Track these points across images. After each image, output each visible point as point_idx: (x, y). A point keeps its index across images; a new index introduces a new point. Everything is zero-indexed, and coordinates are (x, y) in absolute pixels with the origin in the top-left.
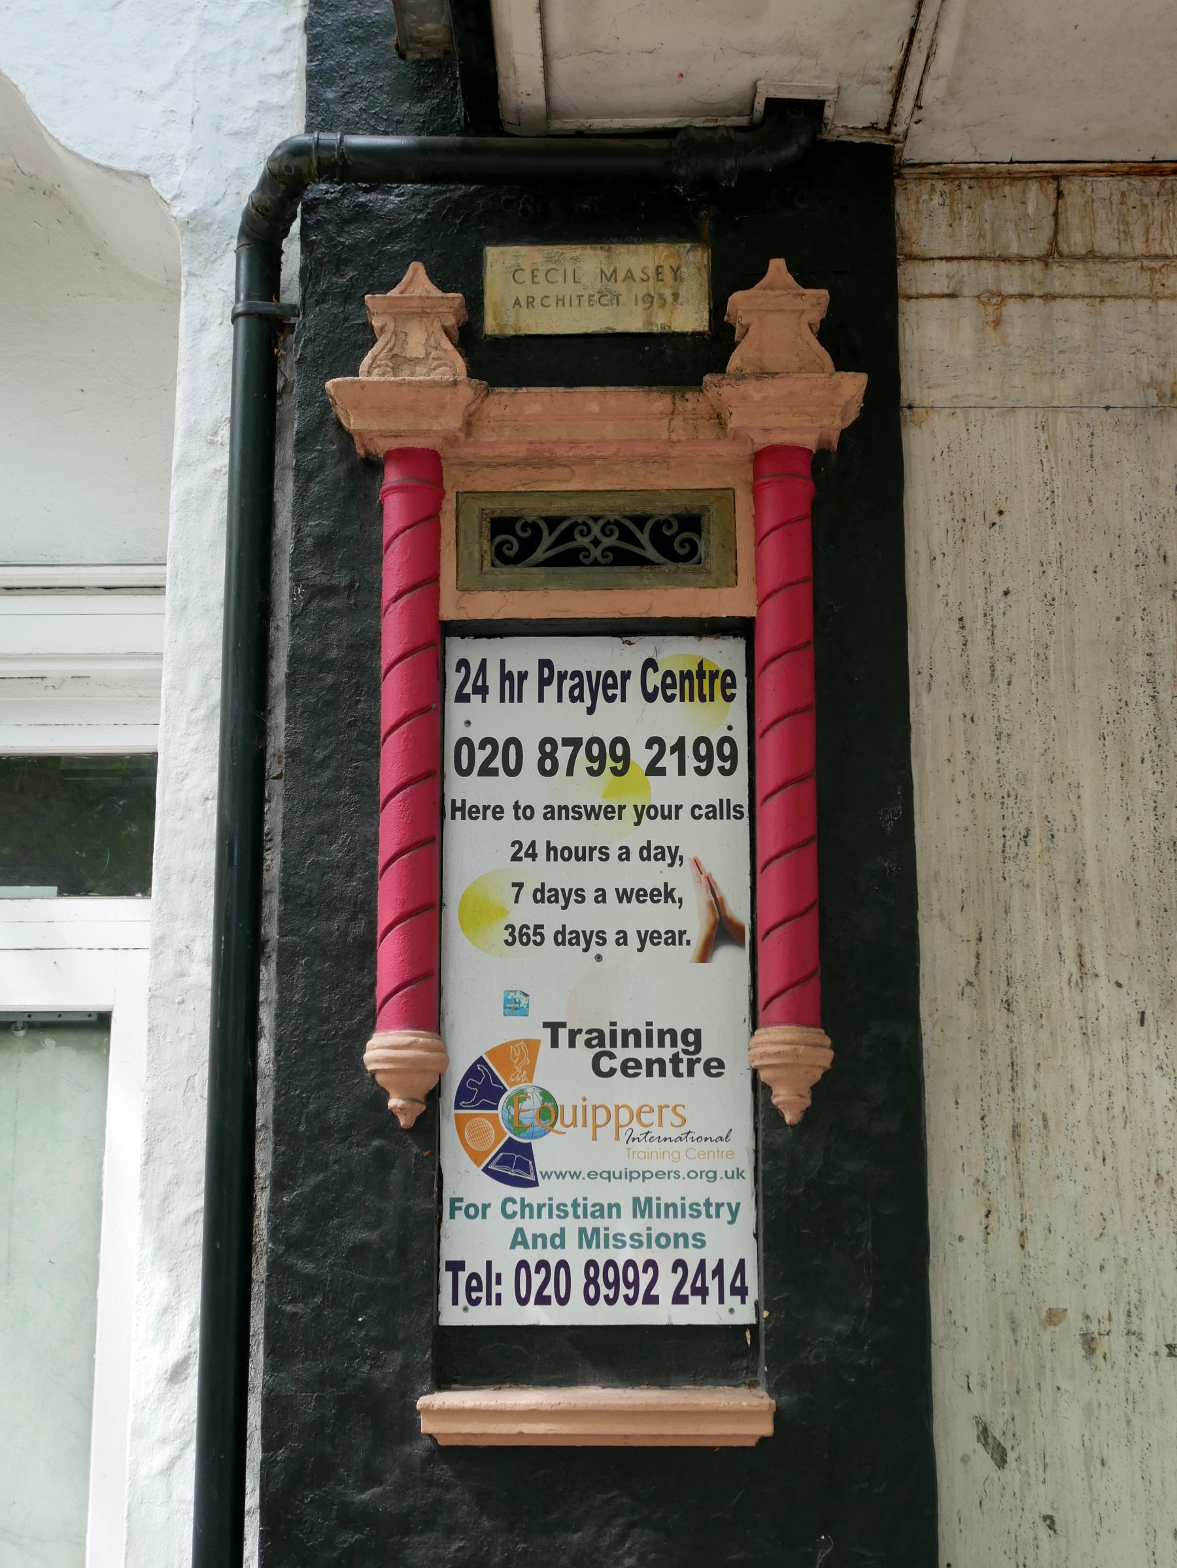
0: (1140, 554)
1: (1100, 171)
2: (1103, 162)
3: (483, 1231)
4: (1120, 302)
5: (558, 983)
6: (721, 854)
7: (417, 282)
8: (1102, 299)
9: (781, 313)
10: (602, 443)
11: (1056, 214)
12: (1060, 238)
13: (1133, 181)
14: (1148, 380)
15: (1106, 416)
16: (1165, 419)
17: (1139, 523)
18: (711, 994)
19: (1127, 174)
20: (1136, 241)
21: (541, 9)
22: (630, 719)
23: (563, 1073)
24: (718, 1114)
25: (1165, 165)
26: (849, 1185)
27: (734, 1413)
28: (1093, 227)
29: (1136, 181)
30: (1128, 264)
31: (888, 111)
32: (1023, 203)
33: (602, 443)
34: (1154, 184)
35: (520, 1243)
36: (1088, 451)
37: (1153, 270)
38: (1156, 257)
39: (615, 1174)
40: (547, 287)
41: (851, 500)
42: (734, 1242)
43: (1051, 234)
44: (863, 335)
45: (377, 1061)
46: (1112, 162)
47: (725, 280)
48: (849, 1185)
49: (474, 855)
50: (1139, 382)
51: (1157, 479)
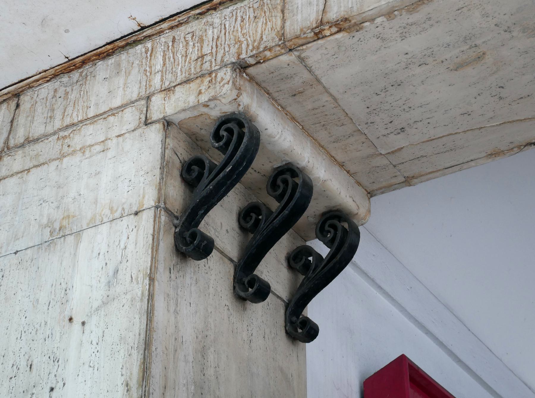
0: (15, 367)
1: (37, 80)
2: (40, 73)
4: (39, 168)
8: (28, 170)
11: (12, 122)
12: (11, 137)
13: (63, 79)
14: (46, 222)
15: (14, 259)
16: (52, 249)
17: (19, 341)
19: (55, 76)
20: (56, 121)
25: (77, 60)
28: (32, 122)
29: (65, 79)
30: (50, 139)
31: (179, 86)
34: (75, 75)
36: (369, 124)
37: (64, 138)
38: (67, 127)
43: (7, 136)
46: (45, 71)
50: (40, 225)
51: (38, 300)
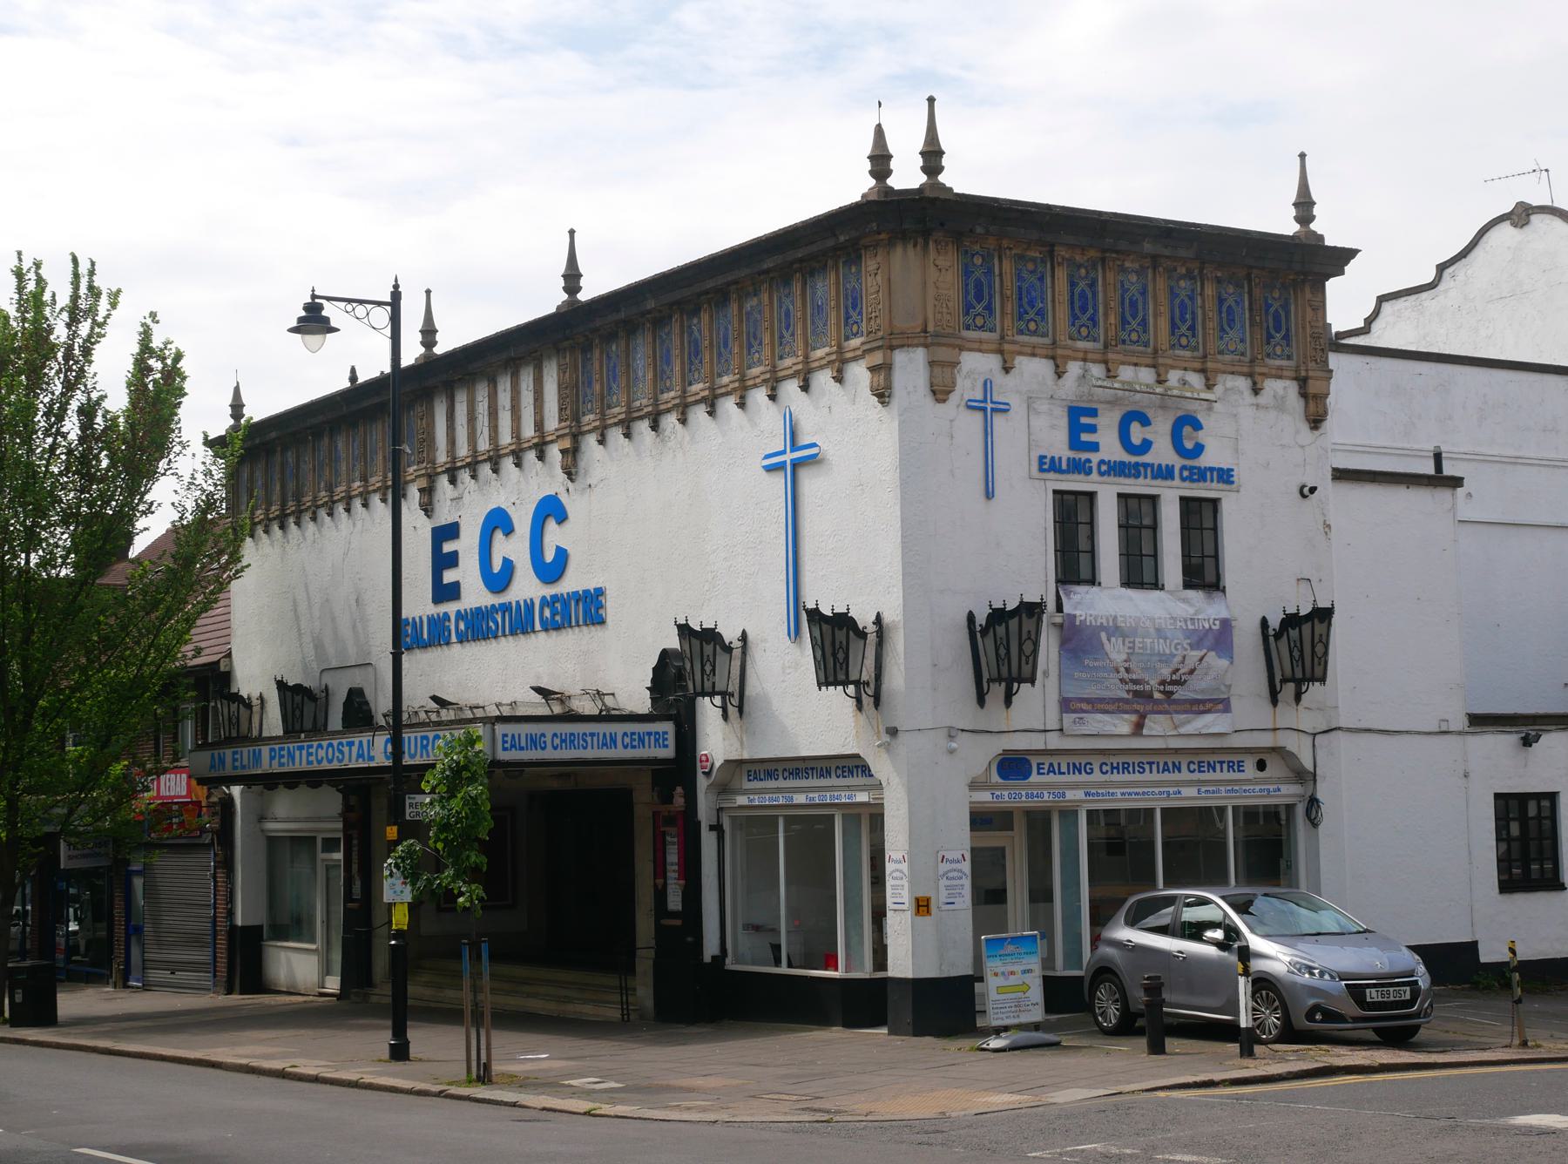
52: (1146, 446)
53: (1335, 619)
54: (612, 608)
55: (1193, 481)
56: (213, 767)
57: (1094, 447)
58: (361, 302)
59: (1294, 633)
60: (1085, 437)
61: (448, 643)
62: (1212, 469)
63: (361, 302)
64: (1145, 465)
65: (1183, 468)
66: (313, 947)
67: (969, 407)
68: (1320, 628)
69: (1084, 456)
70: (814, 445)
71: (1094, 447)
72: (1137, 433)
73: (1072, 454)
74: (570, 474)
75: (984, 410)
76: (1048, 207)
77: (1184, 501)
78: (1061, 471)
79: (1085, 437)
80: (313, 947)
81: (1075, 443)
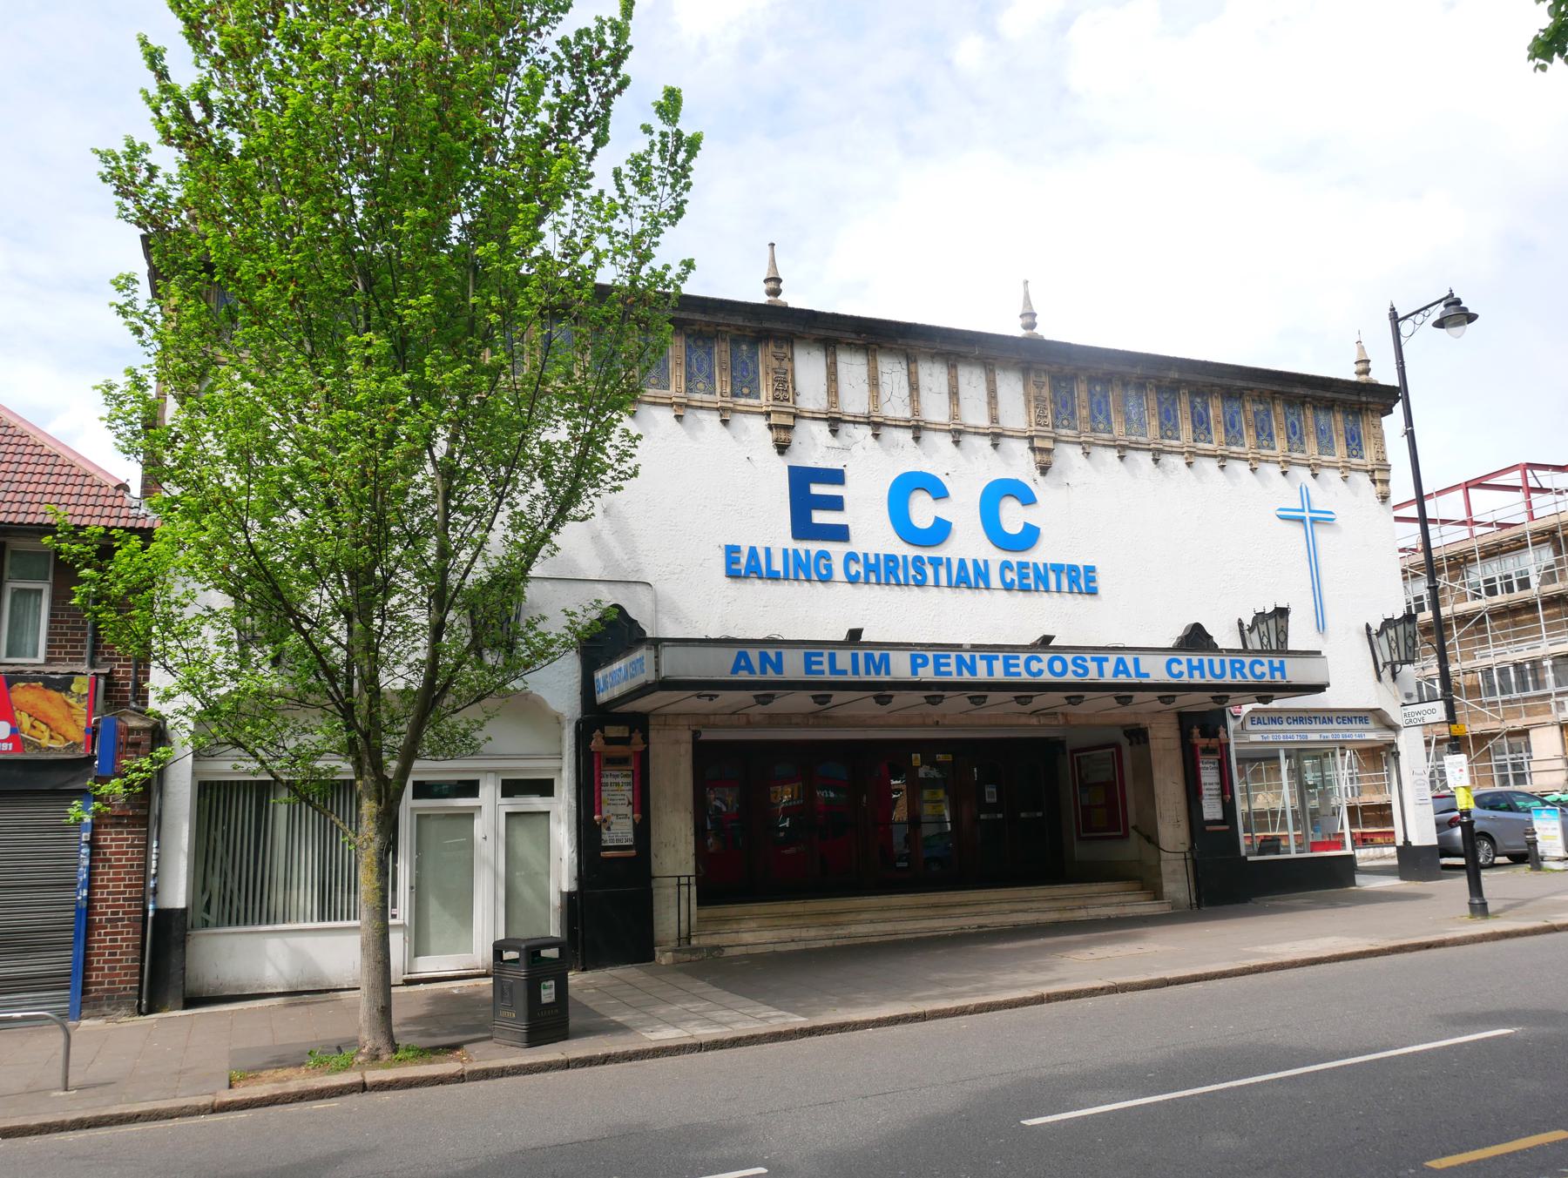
3: (606, 836)
5: (612, 809)
6: (629, 795)
7: (598, 732)
9: (637, 737)
10: (618, 750)
18: (628, 810)
21: (8, 1133)
22: (620, 780)
23: (613, 819)
24: (629, 823)
26: (643, 830)
27: (633, 853)
32: (339, 1049)
33: (618, 750)
35: (743, 668)
39: (619, 832)
40: (613, 731)
41: (643, 758)
42: (631, 836)
44: (646, 739)
45: (403, 1024)
47: (631, 732)
48: (643, 830)
49: (604, 795)
52: (941, 531)
53: (1290, 617)
54: (1102, 583)
55: (1025, 589)
56: (735, 670)
57: (840, 533)
58: (1417, 312)
59: (1263, 628)
60: (820, 517)
61: (826, 579)
62: (1057, 569)
63: (1417, 312)
64: (936, 562)
65: (1006, 566)
66: (357, 923)
67: (1282, 518)
68: (1281, 622)
69: (815, 547)
70: (1398, 519)
71: (840, 533)
72: (923, 511)
73: (792, 545)
74: (1044, 469)
75: (1302, 520)
76: (1068, 345)
77: (415, 797)
78: (774, 577)
79: (820, 517)
80: (357, 923)
81: (803, 528)
